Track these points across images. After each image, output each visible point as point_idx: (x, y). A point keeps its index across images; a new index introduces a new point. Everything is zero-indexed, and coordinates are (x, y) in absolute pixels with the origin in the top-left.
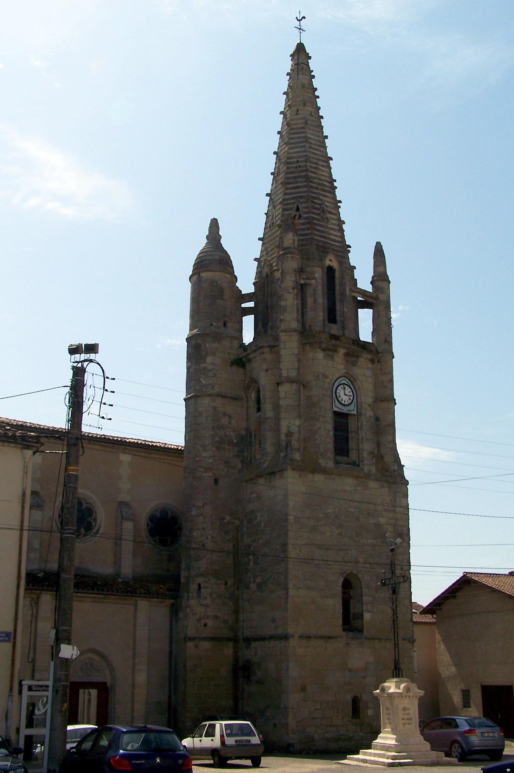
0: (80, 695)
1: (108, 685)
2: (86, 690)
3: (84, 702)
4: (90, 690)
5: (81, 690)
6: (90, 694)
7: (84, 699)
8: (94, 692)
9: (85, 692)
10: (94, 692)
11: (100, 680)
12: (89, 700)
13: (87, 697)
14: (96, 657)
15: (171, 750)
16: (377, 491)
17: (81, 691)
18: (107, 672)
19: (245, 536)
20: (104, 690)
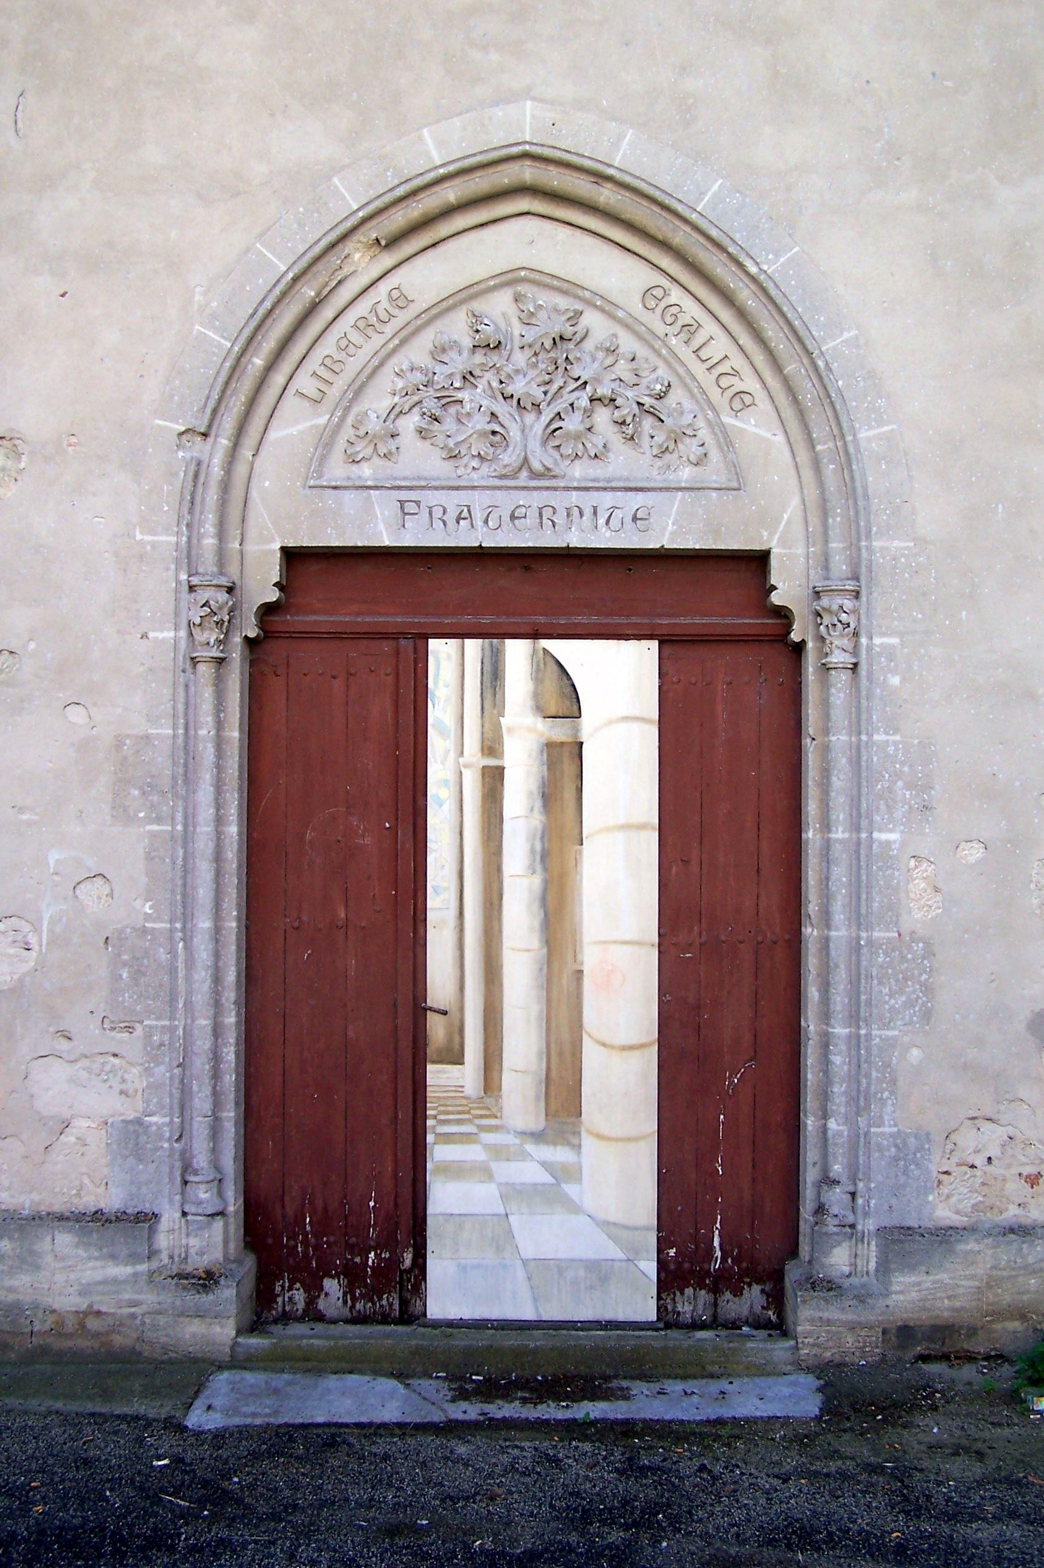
0: (440, 712)
1: (786, 588)
2: (517, 653)
3: (493, 780)
4: (558, 648)
5: (440, 650)
6: (564, 698)
7: (492, 746)
8: (619, 678)
9: (493, 676)
10: (619, 678)
11: (670, 529)
12: (564, 762)
13: (524, 737)
14: (613, 272)
15: (851, 943)
16: (499, 785)
17: (451, 664)
18: (760, 430)
19: (168, 1134)
20: (732, 640)
